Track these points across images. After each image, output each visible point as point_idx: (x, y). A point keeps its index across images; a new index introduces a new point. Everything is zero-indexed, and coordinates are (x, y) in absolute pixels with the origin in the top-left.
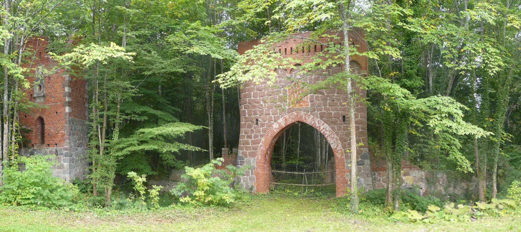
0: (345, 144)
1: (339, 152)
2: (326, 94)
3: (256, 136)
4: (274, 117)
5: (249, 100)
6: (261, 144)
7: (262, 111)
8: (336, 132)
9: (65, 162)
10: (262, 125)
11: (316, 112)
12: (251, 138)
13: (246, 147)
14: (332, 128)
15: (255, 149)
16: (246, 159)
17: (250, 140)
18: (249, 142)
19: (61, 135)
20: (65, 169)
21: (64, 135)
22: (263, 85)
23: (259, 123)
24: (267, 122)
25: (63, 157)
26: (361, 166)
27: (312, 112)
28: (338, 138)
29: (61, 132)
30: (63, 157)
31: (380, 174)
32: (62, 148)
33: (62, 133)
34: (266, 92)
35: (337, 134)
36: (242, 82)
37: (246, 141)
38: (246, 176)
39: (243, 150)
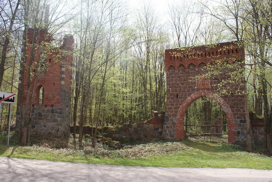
0: (233, 110)
1: (229, 114)
2: (171, 92)
3: (177, 105)
4: (188, 93)
5: (172, 83)
6: (180, 109)
7: (181, 89)
8: (227, 102)
9: (59, 118)
10: (181, 98)
11: (214, 90)
12: (174, 105)
13: (170, 111)
14: (225, 100)
15: (177, 112)
16: (170, 118)
17: (173, 107)
18: (172, 108)
19: (57, 99)
20: (58, 123)
21: (59, 99)
22: (181, 75)
23: (179, 96)
24: (184, 96)
25: (57, 114)
26: (245, 123)
27: (211, 91)
28: (229, 106)
29: (56, 97)
30: (57, 114)
31: (256, 128)
32: (57, 108)
33: (57, 98)
34: (183, 78)
35: (228, 103)
36: (5, 157)
37: (170, 107)
38: (170, 129)
39: (168, 113)
